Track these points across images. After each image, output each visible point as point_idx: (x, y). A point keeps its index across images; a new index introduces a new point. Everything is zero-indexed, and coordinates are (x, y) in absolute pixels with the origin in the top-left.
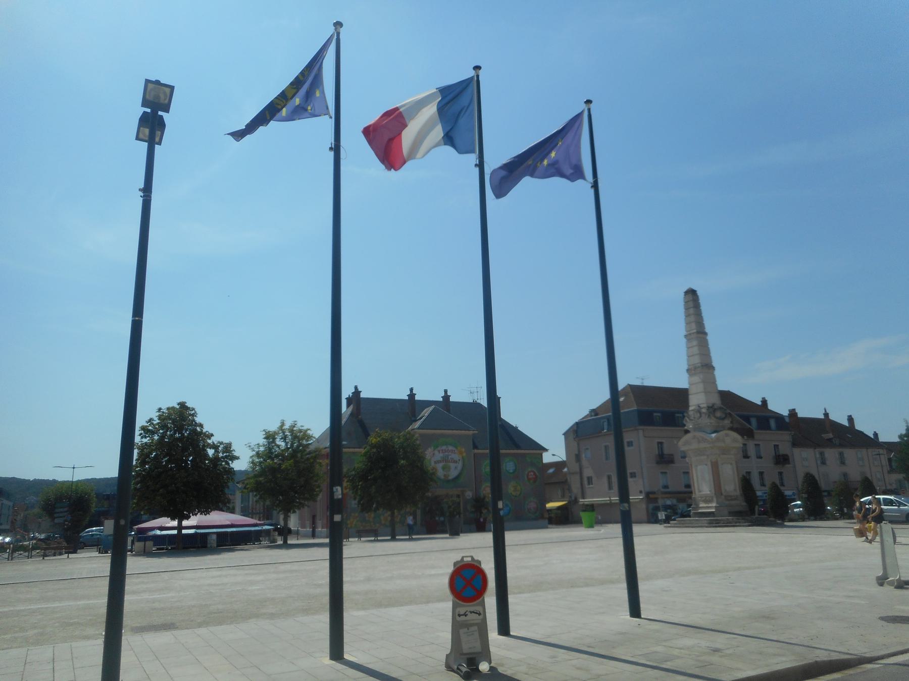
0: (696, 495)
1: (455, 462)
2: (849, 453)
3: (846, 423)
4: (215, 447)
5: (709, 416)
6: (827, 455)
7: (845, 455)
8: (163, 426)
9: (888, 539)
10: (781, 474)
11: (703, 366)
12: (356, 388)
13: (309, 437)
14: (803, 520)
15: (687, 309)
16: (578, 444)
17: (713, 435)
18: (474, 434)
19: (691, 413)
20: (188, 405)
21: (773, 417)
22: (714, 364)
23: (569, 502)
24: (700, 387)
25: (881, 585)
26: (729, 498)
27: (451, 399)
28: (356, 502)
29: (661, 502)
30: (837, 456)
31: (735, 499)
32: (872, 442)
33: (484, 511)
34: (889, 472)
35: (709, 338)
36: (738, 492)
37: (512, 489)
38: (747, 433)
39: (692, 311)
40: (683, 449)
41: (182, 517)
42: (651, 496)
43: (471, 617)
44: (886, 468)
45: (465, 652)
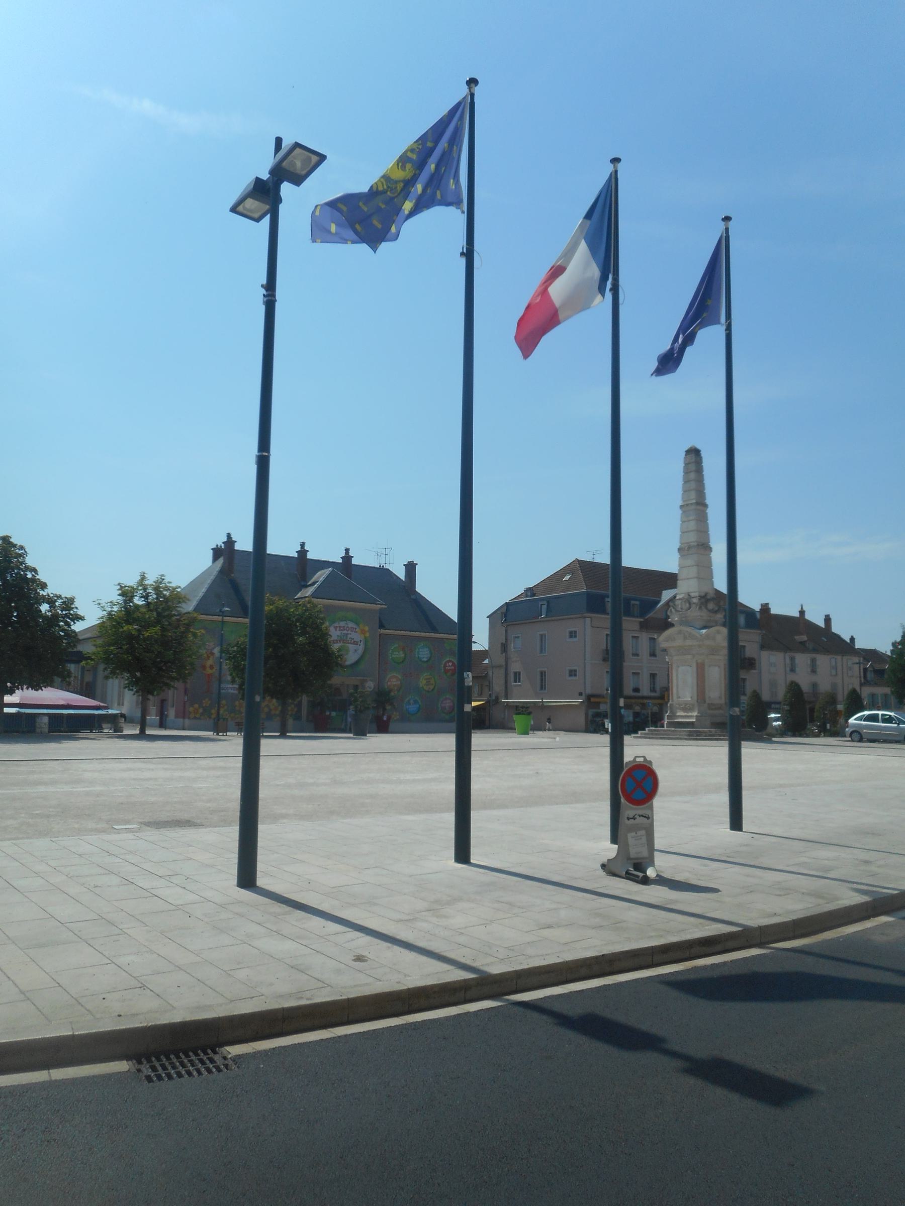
1: (356, 643)
2: (823, 661)
3: (822, 624)
4: (51, 601)
5: (700, 608)
6: (797, 661)
7: (818, 663)
12: (229, 536)
13: (177, 597)
16: (506, 631)
17: (704, 631)
18: (381, 609)
20: (13, 540)
21: (742, 612)
23: (488, 702)
24: (693, 572)
26: (711, 706)
27: (354, 562)
30: (809, 662)
31: (720, 708)
32: (846, 648)
33: (388, 707)
35: (709, 511)
37: (425, 682)
39: (692, 476)
40: (664, 645)
42: (593, 700)
43: (639, 820)
45: (632, 856)
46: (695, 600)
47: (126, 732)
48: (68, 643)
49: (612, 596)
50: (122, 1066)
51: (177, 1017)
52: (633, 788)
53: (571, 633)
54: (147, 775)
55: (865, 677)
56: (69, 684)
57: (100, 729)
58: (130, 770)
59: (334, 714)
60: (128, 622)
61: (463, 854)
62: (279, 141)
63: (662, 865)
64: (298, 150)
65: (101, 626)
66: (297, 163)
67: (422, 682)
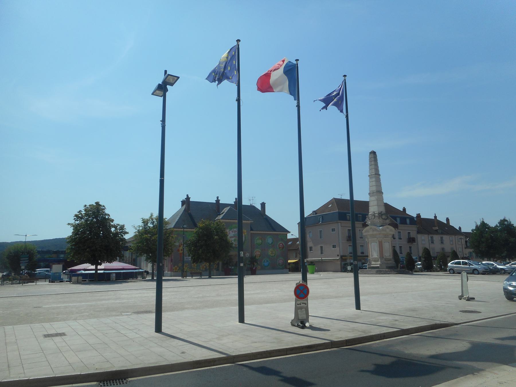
0: (370, 257)
2: (446, 238)
4: (115, 227)
6: (434, 239)
8: (86, 215)
9: (465, 279)
10: (410, 247)
11: (378, 192)
12: (187, 195)
14: (422, 272)
15: (370, 161)
19: (370, 216)
20: (100, 203)
22: (383, 191)
24: (375, 203)
25: (460, 299)
26: (387, 260)
28: (190, 257)
29: (348, 261)
33: (255, 264)
34: (465, 248)
36: (391, 257)
38: (395, 226)
39: (373, 163)
41: (97, 264)
42: (343, 258)
43: (302, 305)
44: (464, 246)
46: (376, 215)
47: (147, 279)
48: (122, 244)
49: (348, 213)
50: (95, 383)
51: (114, 369)
52: (302, 292)
53: (332, 229)
54: (146, 295)
55: (466, 245)
56: (123, 260)
57: (137, 278)
58: (140, 293)
59: (233, 268)
60: (146, 233)
61: (242, 319)
62: (166, 71)
63: (312, 321)
64: (169, 76)
65: (135, 236)
66: (171, 80)
67: (270, 253)
